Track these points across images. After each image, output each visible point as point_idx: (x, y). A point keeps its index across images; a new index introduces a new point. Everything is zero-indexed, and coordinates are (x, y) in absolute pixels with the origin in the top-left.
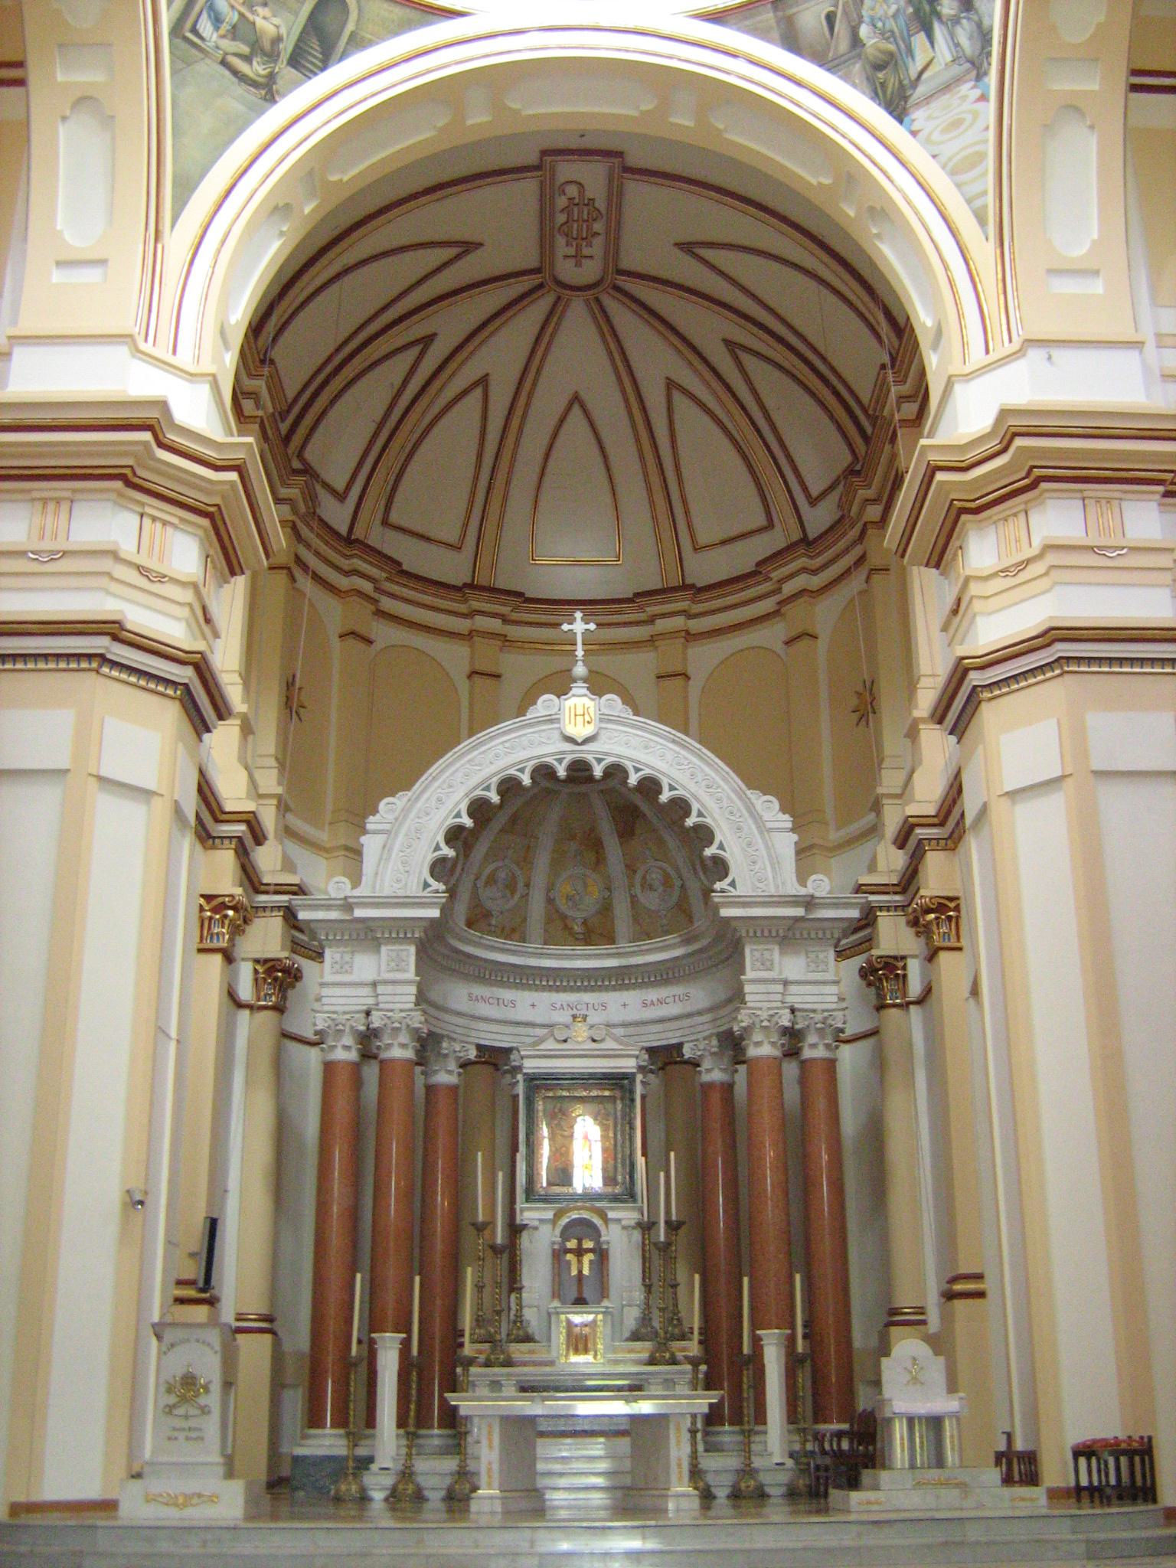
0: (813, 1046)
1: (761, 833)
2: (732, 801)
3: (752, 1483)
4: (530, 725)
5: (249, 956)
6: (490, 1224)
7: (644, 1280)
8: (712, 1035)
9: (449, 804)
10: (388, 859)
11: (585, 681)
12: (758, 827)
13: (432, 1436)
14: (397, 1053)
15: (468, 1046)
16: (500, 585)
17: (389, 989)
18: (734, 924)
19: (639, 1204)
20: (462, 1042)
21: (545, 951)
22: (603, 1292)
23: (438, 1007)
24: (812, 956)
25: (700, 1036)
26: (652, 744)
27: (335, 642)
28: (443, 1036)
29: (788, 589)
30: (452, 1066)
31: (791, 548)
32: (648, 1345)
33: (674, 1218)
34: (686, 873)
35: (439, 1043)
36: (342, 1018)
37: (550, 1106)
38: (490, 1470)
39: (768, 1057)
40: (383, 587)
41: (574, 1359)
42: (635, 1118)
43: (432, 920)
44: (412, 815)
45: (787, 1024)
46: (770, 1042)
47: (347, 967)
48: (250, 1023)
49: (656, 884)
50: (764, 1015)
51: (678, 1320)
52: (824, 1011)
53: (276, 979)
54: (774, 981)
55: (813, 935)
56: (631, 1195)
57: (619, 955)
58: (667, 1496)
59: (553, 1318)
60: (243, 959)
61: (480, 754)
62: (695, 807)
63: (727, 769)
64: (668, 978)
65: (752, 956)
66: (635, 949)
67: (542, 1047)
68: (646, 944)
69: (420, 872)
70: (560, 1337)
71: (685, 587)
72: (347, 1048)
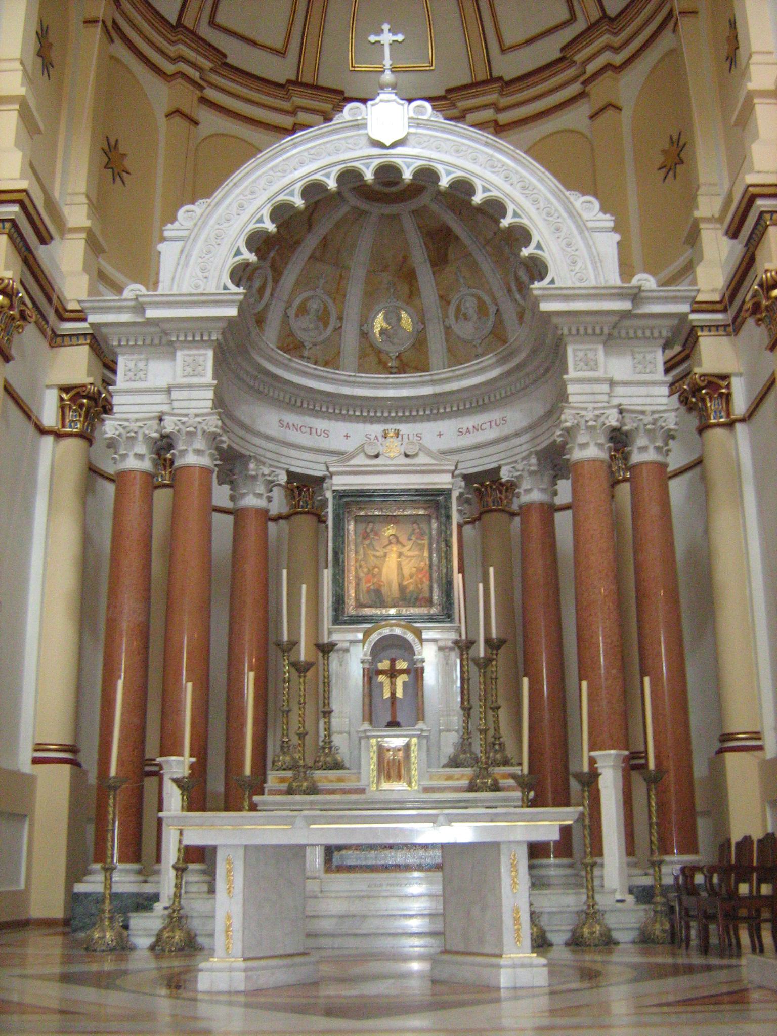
0: (643, 449)
1: (581, 232)
2: (549, 202)
3: (597, 928)
4: (336, 131)
5: (54, 383)
6: (294, 644)
8: (531, 453)
9: (251, 210)
10: (186, 265)
11: (394, 87)
12: (578, 226)
13: (548, 866)
14: (191, 459)
15: (278, 471)
16: (322, 83)
17: (185, 394)
18: (555, 320)
20: (271, 466)
21: (358, 380)
22: (419, 714)
23: (243, 426)
24: (639, 357)
25: (518, 457)
26: (464, 148)
27: (162, 122)
29: (591, 68)
30: (261, 489)
31: (592, 27)
32: (468, 771)
33: (494, 636)
34: (500, 294)
36: (134, 426)
37: (362, 526)
38: (227, 929)
39: (595, 461)
40: (207, 78)
41: (385, 786)
42: (451, 535)
43: (230, 320)
44: (212, 222)
45: (615, 424)
46: (596, 444)
47: (141, 374)
48: (53, 450)
49: (471, 312)
50: (589, 415)
51: (500, 744)
52: (653, 412)
53: (81, 406)
54: (597, 381)
55: (640, 334)
56: (447, 614)
57: (433, 382)
58: (499, 966)
59: (363, 742)
60: (48, 387)
61: (284, 160)
62: (511, 208)
63: (543, 170)
65: (575, 356)
66: (451, 374)
67: (352, 462)
68: (460, 370)
69: (220, 278)
70: (370, 765)
71: (492, 80)
72: (140, 457)
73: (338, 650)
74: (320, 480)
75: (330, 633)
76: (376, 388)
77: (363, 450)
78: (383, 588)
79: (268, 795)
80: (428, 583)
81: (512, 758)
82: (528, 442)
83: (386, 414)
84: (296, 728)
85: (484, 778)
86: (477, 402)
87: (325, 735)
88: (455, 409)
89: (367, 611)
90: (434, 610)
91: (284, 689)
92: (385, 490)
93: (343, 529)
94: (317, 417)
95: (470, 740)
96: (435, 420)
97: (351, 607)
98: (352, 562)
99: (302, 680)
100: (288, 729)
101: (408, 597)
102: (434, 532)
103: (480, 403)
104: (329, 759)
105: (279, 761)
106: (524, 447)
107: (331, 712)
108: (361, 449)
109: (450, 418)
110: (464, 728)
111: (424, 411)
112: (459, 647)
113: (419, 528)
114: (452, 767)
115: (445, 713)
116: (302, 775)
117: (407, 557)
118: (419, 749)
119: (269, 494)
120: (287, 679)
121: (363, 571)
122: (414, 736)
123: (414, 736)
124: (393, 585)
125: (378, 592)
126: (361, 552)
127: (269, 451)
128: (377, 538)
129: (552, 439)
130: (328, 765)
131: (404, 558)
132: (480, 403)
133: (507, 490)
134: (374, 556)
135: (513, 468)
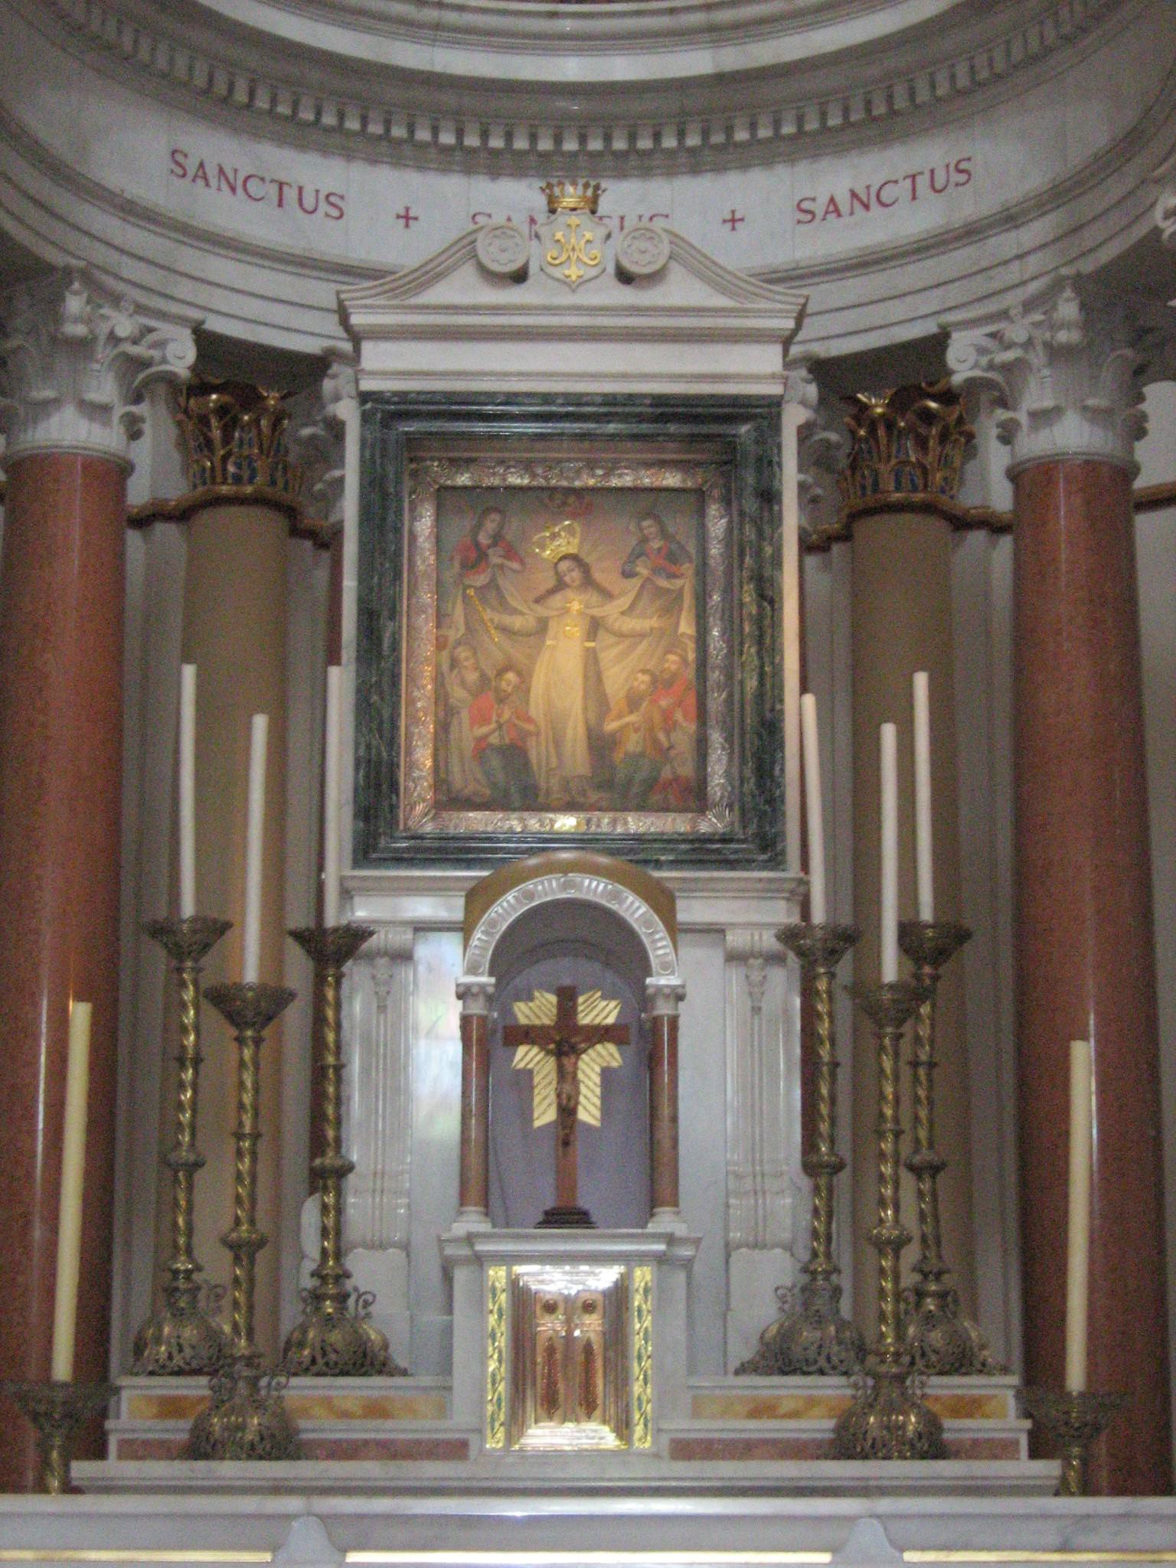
7: (809, 1144)
8: (1057, 286)
15: (165, 329)
19: (793, 870)
20: (140, 309)
28: (68, 273)
30: (105, 388)
32: (833, 1388)
33: (926, 914)
35: (55, 301)
37: (459, 528)
42: (777, 561)
59: (460, 1275)
64: (893, 113)
67: (436, 295)
73: (371, 957)
74: (318, 366)
75: (346, 894)
76: (510, 49)
77: (474, 255)
78: (532, 743)
79: (120, 1457)
80: (692, 727)
81: (983, 1347)
82: (1043, 246)
83: (545, 145)
84: (227, 1223)
85: (891, 1409)
86: (868, 105)
87: (324, 1252)
88: (788, 129)
89: (477, 821)
90: (710, 824)
91: (181, 1086)
92: (547, 398)
93: (398, 530)
94: (302, 146)
95: (834, 1277)
96: (720, 168)
97: (420, 808)
98: (427, 649)
99: (247, 1053)
100: (190, 1231)
101: (621, 775)
102: (715, 550)
103: (880, 109)
104: (335, 1337)
105: (158, 1340)
106: (1033, 263)
107: (344, 1170)
108: (465, 249)
109: (768, 162)
110: (815, 1234)
111: (681, 135)
112: (801, 953)
113: (663, 533)
114: (769, 1372)
115: (748, 1183)
116: (242, 1387)
117: (622, 636)
118: (658, 1311)
119: (134, 409)
120: (191, 1052)
121: (463, 684)
122: (641, 1258)
123: (641, 1258)
124: (570, 732)
125: (515, 755)
126: (458, 613)
127: (133, 255)
128: (516, 566)
129: (1140, 231)
130: (333, 1357)
131: (612, 639)
132: (880, 109)
133: (944, 438)
134: (505, 630)
135: (993, 335)
